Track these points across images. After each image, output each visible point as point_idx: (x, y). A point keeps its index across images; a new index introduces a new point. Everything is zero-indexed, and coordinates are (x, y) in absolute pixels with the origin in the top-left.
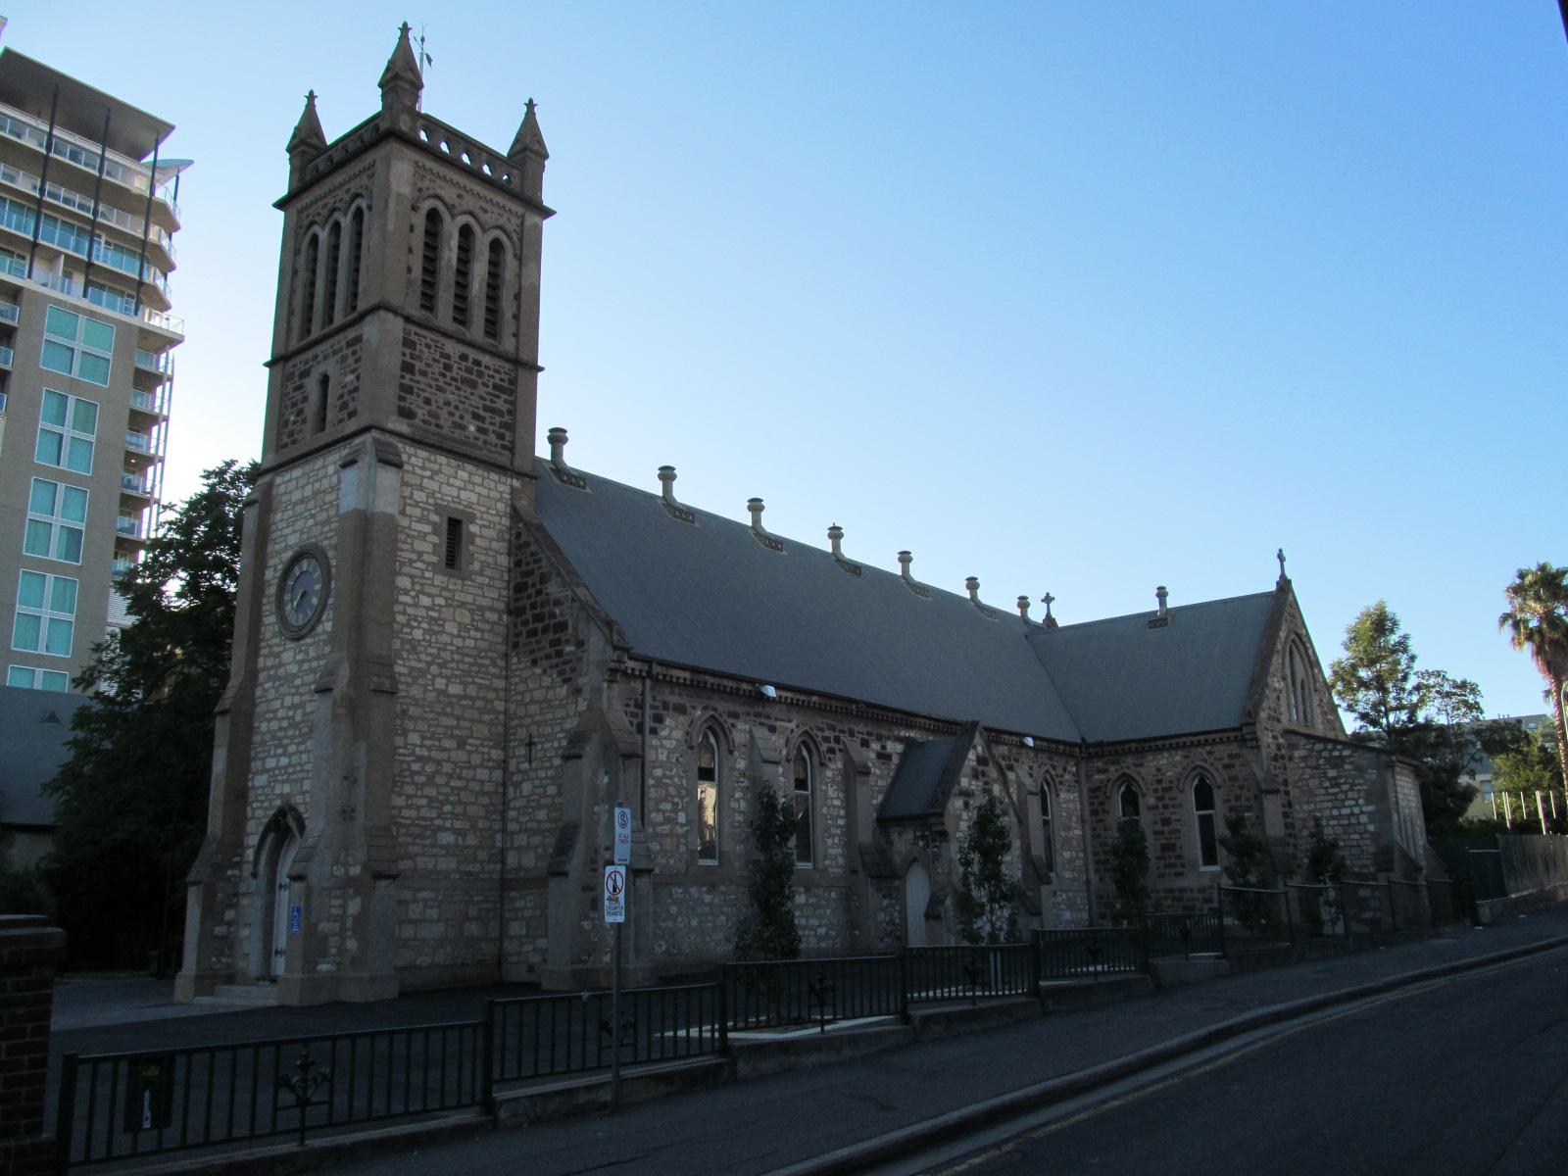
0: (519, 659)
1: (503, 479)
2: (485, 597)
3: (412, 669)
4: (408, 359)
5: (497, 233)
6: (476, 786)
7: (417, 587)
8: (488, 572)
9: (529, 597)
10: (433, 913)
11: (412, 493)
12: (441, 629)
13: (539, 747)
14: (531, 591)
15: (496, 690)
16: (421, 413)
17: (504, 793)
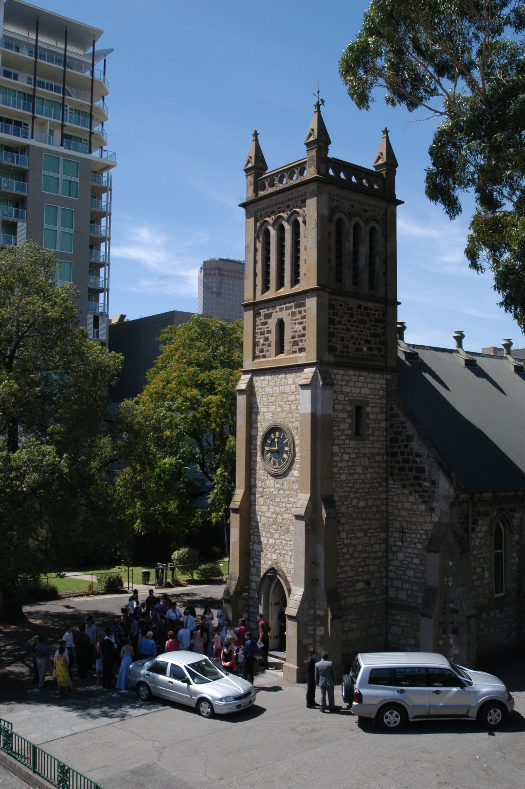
0: (394, 482)
1: (382, 376)
2: (374, 448)
3: (341, 497)
4: (331, 316)
5: (373, 224)
6: (373, 555)
7: (342, 450)
8: (376, 433)
9: (399, 447)
10: (355, 626)
11: (337, 397)
12: (354, 471)
13: (408, 535)
14: (400, 444)
15: (382, 500)
16: (339, 347)
17: (387, 556)
